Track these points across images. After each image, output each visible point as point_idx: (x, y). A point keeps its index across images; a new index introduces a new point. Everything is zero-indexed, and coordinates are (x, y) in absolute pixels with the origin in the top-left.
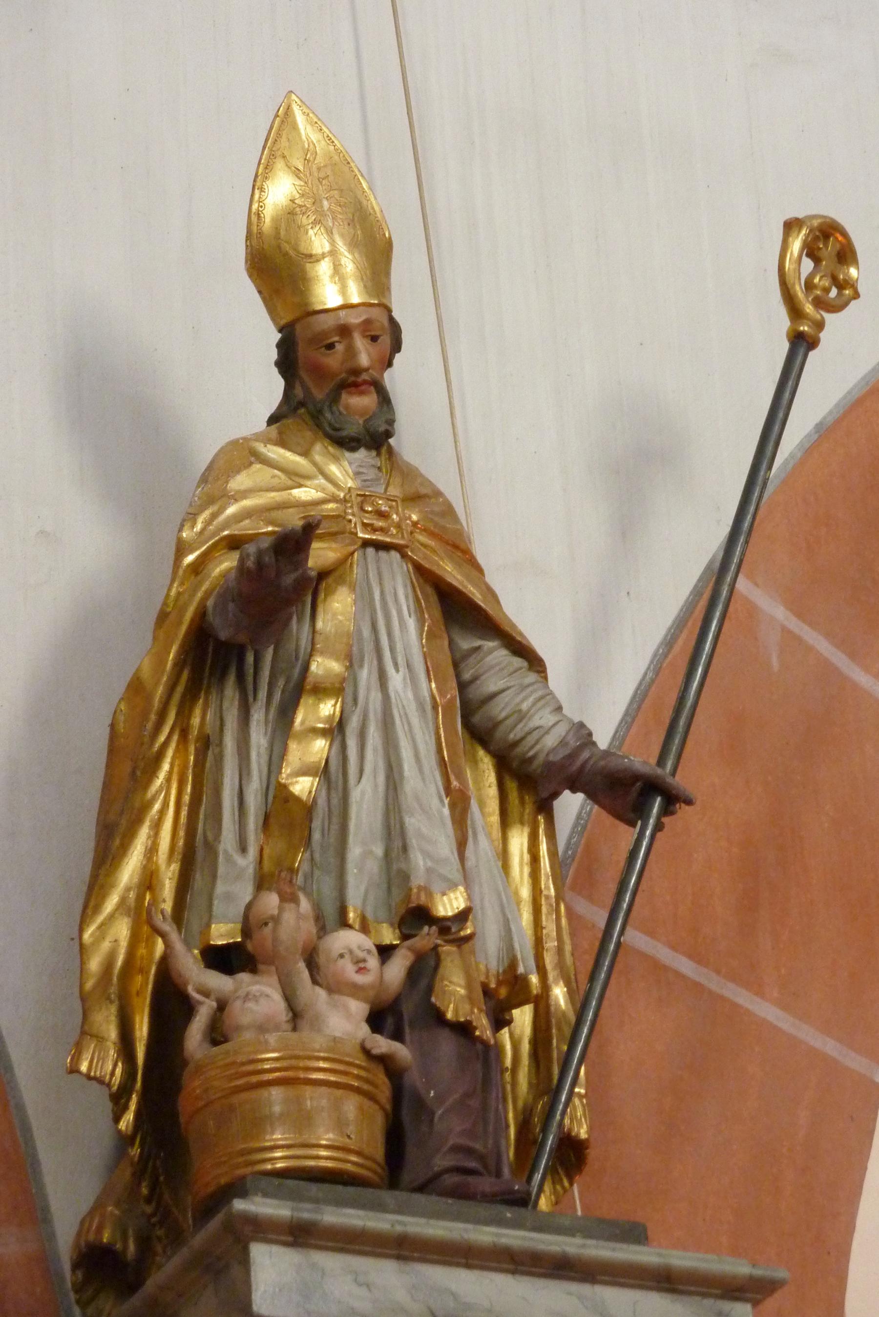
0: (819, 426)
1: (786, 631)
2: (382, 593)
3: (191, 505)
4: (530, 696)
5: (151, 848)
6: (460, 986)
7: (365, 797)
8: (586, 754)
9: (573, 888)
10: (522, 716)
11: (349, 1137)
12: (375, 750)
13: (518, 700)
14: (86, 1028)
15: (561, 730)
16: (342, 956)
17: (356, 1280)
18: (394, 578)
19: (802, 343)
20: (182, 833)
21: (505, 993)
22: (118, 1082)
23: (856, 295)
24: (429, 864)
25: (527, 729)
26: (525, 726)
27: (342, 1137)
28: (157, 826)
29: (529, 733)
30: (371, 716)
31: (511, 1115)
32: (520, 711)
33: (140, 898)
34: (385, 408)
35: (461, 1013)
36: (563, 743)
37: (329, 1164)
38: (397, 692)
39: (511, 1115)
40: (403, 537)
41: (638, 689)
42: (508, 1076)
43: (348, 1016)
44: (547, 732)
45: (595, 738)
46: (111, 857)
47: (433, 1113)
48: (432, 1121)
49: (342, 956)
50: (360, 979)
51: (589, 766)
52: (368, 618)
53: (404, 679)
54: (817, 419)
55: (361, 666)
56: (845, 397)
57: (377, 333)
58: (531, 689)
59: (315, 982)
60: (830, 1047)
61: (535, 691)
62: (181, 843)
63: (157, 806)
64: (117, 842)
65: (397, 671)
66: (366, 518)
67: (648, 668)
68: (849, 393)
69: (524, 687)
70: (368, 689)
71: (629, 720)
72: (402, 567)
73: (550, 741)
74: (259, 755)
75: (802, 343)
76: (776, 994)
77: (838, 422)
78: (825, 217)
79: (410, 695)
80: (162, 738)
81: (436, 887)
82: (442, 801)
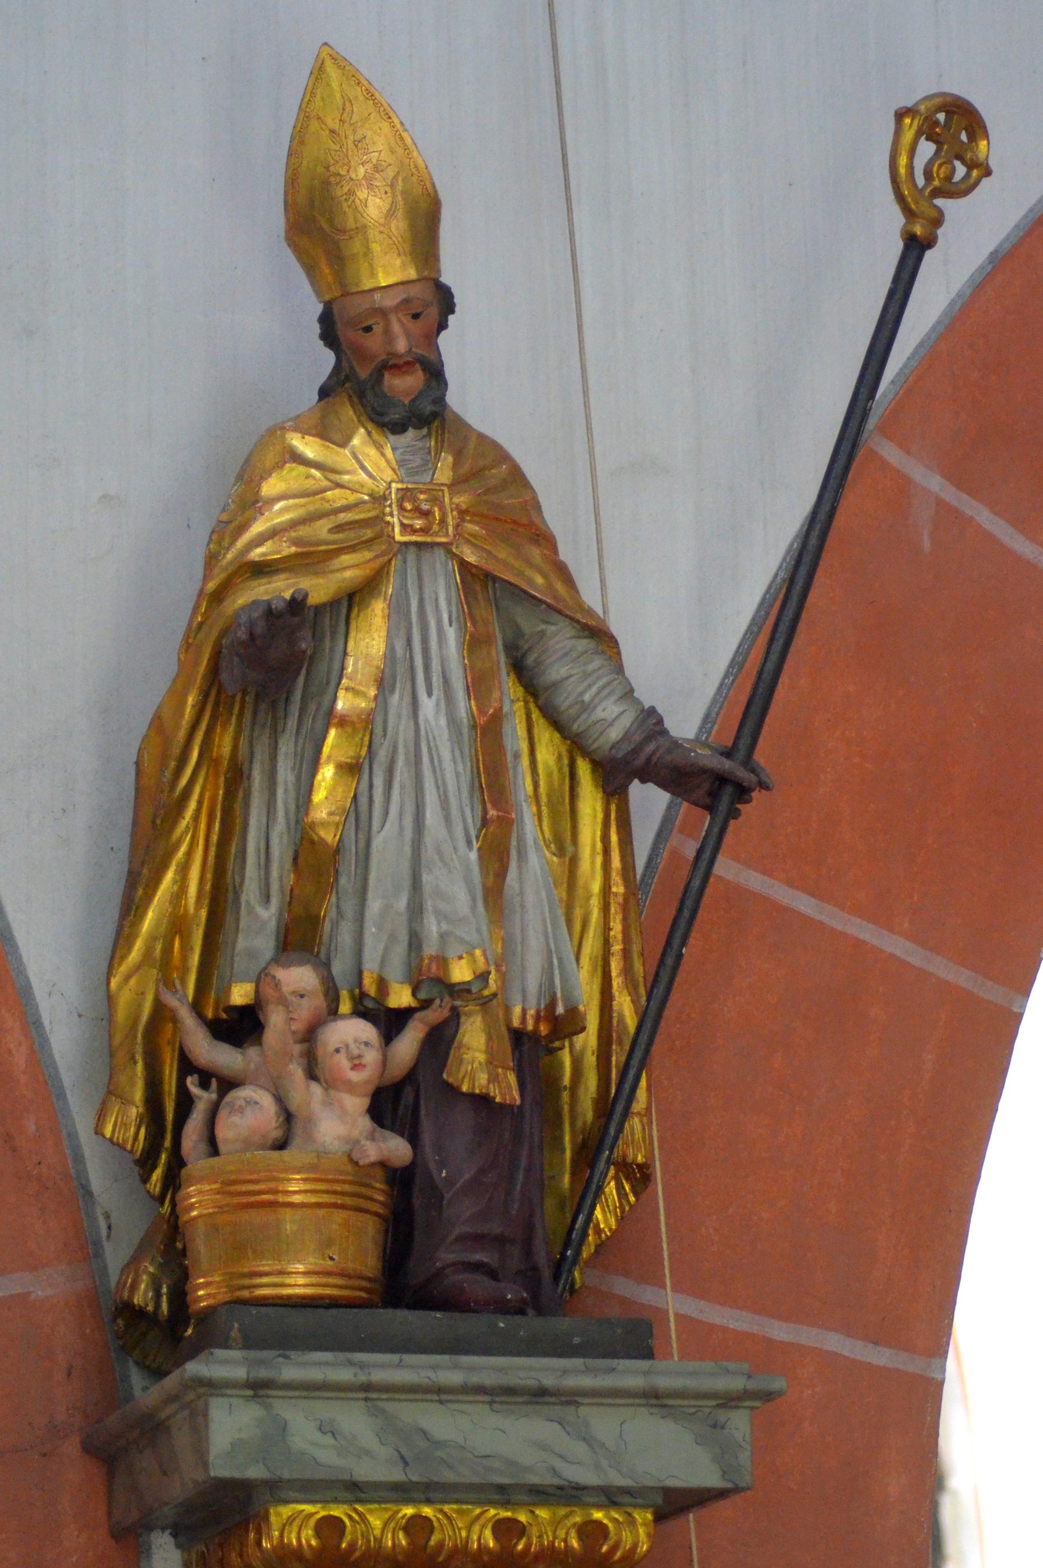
0: (993, 255)
1: (941, 503)
2: (421, 601)
3: (223, 510)
4: (594, 684)
5: (182, 882)
6: (479, 1051)
7: (388, 843)
8: (651, 747)
9: (682, 831)
10: (586, 708)
11: (331, 1259)
12: (402, 787)
13: (581, 689)
14: (111, 1087)
15: (626, 721)
16: (337, 1051)
17: (320, 1429)
18: (436, 580)
19: (916, 246)
20: (209, 876)
21: (531, 1049)
22: (141, 1147)
23: (988, 173)
24: (445, 927)
25: (590, 721)
26: (588, 718)
27: (324, 1259)
28: (184, 870)
29: (595, 723)
30: (401, 750)
31: (567, 1138)
32: (583, 702)
33: (168, 950)
34: (434, 384)
35: (477, 1084)
36: (626, 737)
37: (309, 1291)
38: (427, 721)
39: (567, 1138)
40: (447, 535)
41: (768, 591)
42: (565, 1096)
43: (344, 1112)
44: (611, 724)
45: (668, 724)
46: (134, 907)
47: (442, 1197)
48: (441, 1206)
49: (337, 1051)
50: (355, 1076)
51: (655, 759)
52: (402, 633)
53: (438, 704)
54: (991, 248)
55: (392, 691)
56: (1026, 216)
57: (419, 310)
58: (595, 675)
59: (312, 1075)
60: (962, 977)
61: (599, 678)
62: (208, 887)
63: (183, 849)
64: (140, 892)
65: (430, 694)
66: (407, 518)
67: (780, 567)
68: (1031, 210)
69: (586, 675)
70: (399, 716)
71: (755, 629)
72: (447, 564)
73: (615, 734)
74: (286, 790)
75: (916, 246)
76: (906, 925)
77: (1016, 247)
78: (943, 94)
79: (443, 722)
80: (184, 781)
81: (451, 953)
82: (469, 843)
